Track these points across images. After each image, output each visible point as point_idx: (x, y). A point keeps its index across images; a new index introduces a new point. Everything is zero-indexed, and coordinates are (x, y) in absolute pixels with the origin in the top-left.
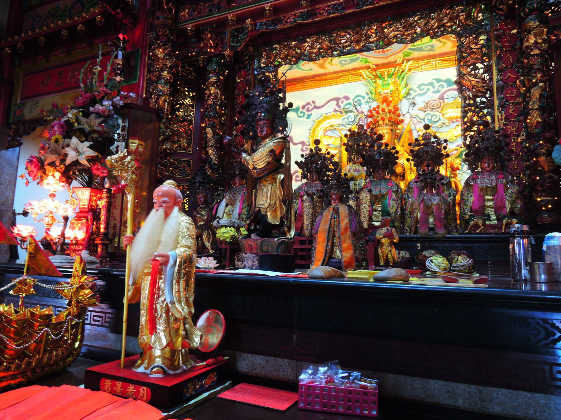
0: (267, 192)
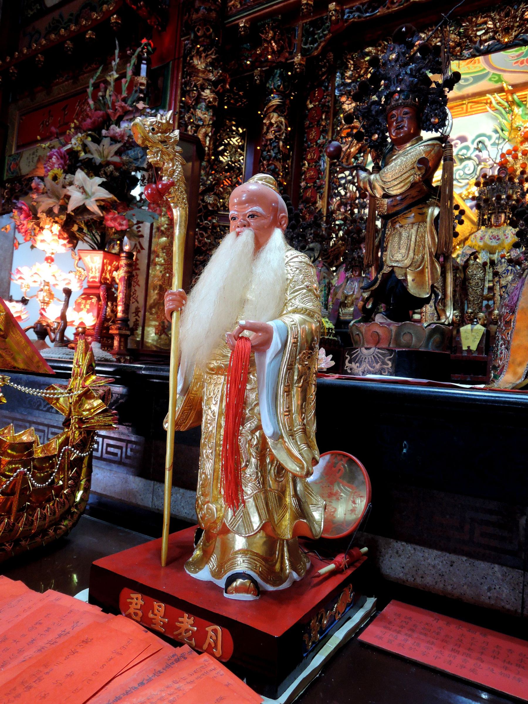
0: (409, 238)
